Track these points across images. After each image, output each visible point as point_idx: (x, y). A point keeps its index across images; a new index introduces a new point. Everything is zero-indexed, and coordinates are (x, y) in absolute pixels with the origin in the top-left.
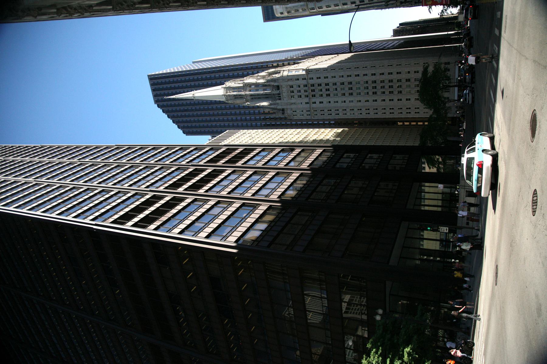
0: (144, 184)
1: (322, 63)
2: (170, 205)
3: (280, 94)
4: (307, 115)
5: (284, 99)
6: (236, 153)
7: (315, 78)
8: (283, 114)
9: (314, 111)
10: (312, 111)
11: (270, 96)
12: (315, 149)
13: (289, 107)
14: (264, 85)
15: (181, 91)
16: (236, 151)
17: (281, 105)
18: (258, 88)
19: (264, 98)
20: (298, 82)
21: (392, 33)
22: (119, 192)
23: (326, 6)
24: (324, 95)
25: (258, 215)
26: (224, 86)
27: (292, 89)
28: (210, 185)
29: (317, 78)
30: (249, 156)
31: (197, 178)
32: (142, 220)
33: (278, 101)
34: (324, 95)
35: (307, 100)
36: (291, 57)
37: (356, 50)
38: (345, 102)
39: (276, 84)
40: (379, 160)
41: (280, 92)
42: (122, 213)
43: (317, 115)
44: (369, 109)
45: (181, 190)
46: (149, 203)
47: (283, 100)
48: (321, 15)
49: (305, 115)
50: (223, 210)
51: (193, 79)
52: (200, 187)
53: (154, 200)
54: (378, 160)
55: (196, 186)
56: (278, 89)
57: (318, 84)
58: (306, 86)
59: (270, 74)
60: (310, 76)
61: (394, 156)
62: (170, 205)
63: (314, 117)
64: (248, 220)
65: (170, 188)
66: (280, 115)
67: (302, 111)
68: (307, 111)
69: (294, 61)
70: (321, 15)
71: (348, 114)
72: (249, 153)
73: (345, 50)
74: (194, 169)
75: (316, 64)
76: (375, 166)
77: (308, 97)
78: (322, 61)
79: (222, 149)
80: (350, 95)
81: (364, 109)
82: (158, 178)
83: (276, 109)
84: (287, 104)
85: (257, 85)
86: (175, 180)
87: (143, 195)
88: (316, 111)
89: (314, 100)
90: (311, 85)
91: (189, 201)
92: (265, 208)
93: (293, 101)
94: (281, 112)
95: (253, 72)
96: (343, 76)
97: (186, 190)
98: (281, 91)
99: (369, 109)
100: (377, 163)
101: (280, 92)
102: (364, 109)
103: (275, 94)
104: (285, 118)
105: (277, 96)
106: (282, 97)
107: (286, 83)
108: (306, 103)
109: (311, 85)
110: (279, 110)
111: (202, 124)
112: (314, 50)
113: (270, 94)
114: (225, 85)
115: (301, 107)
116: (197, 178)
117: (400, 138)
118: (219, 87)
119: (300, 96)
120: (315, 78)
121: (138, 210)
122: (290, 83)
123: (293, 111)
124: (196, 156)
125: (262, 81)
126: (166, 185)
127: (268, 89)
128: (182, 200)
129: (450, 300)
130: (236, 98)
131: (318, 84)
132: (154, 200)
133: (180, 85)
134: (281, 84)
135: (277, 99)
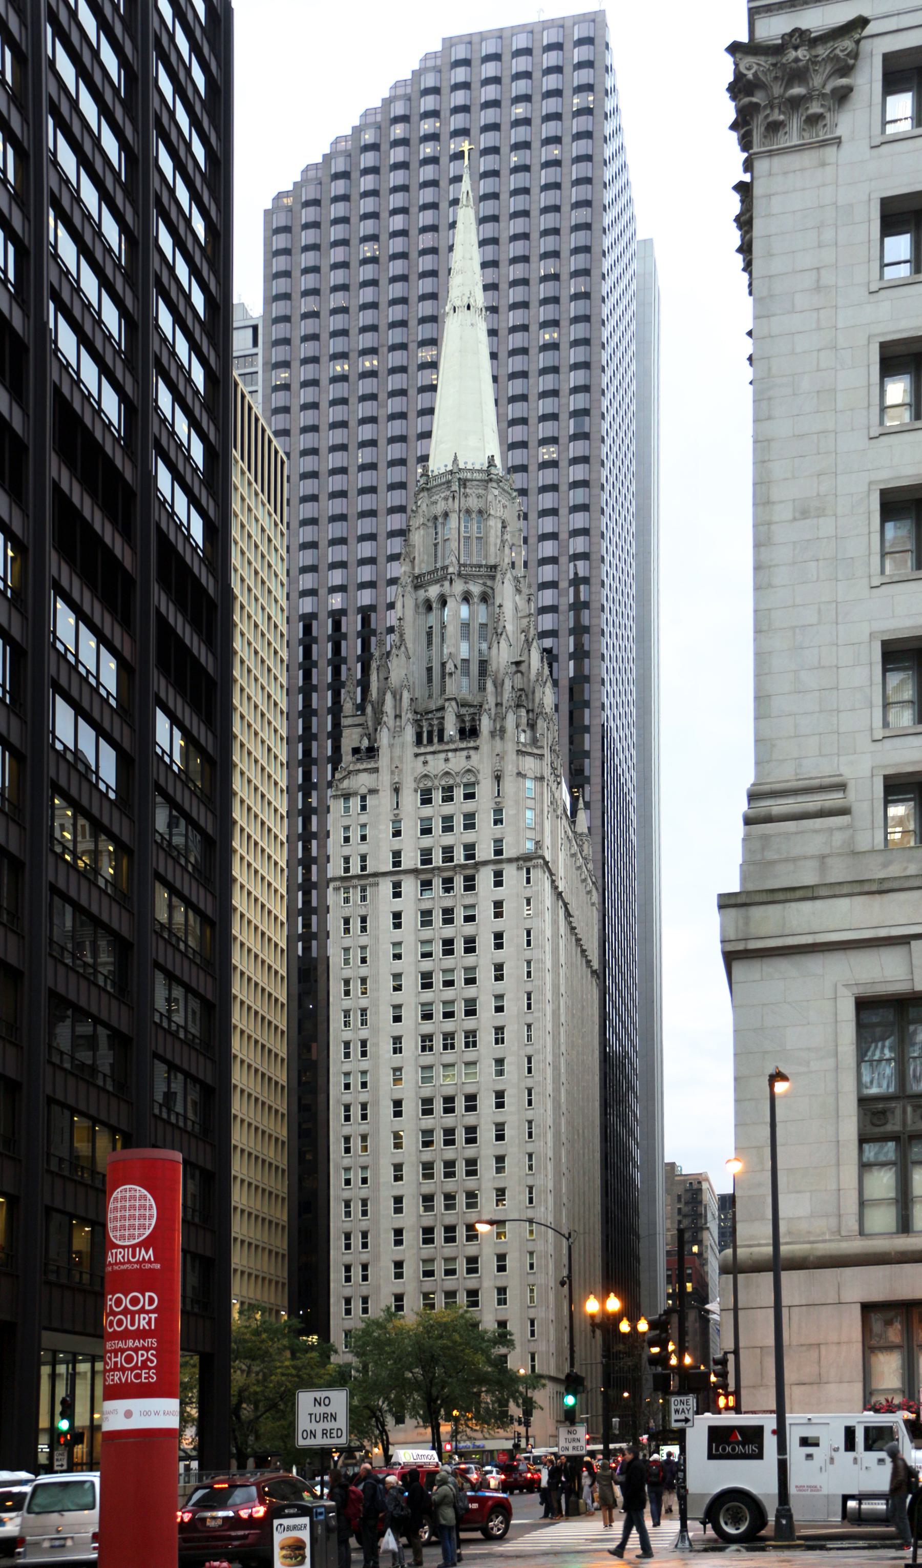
1: (562, 912)
3: (441, 740)
4: (347, 860)
5: (422, 758)
7: (500, 893)
8: (356, 751)
13: (385, 780)
17: (391, 746)
18: (475, 635)
21: (687, 1168)
24: (427, 1027)
34: (427, 1027)
35: (411, 860)
38: (397, 957)
39: (486, 725)
40: (181, 1124)
48: (97, 1530)
53: (120, 518)
54: (181, 1119)
57: (426, 1241)
61: (197, 1173)
66: (351, 738)
76: (177, 1119)
77: (424, 862)
80: (423, 1041)
83: (378, 722)
84: (396, 769)
93: (410, 799)
94: (365, 743)
100: (189, 1123)
101: (452, 741)
104: (336, 760)
105: (431, 725)
106: (430, 749)
110: (372, 738)
115: (383, 836)
117: (277, 1196)
119: (426, 831)
120: (500, 893)
122: (486, 789)
123: (363, 798)
130: (429, 635)
131: (426, 1241)
132: (120, 518)
135: (421, 727)
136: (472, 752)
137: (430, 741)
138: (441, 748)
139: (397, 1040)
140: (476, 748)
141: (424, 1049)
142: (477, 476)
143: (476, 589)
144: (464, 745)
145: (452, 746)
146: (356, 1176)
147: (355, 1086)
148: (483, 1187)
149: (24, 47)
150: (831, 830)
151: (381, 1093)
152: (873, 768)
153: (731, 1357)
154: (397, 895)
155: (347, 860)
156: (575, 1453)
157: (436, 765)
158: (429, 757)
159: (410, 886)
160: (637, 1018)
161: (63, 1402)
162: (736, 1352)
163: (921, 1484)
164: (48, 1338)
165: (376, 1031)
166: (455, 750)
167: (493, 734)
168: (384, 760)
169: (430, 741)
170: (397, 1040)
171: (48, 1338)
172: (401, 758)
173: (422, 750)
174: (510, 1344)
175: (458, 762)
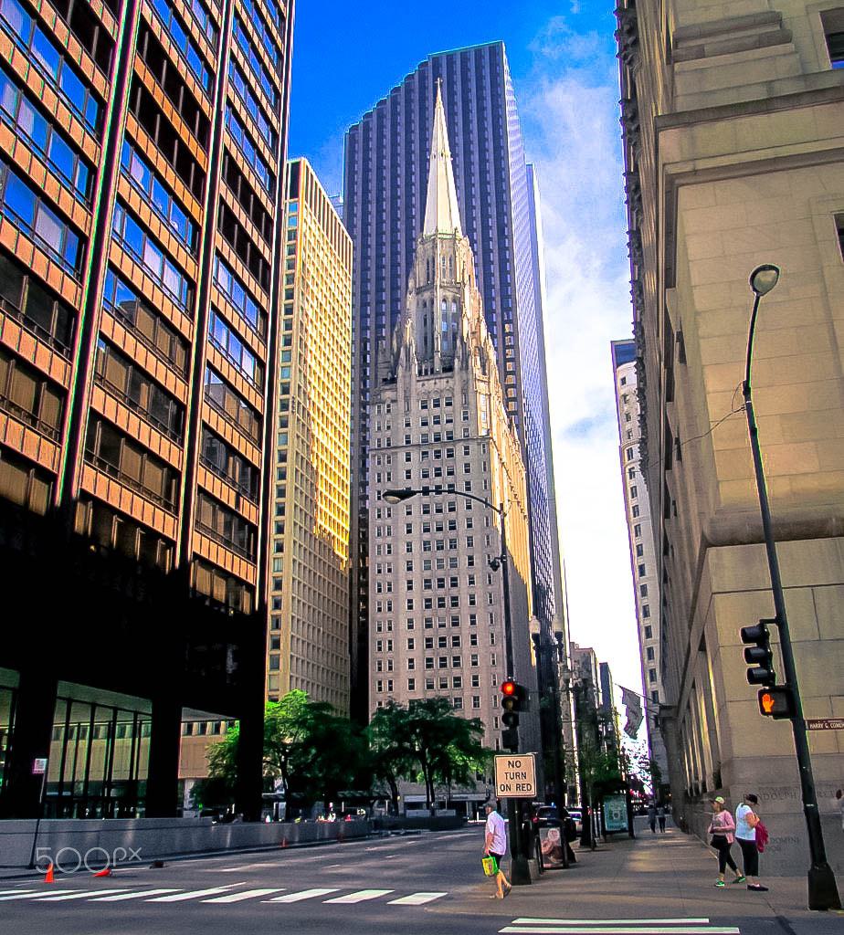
0: (237, 92)
2: (185, 164)
3: (432, 372)
4: (379, 440)
5: (421, 383)
6: (255, 240)
8: (385, 380)
9: (389, 457)
10: (389, 452)
11: (429, 350)
12: (261, 448)
13: (401, 394)
14: (454, 336)
15: (457, 170)
16: (262, 242)
17: (404, 377)
19: (426, 334)
20: (459, 418)
22: (216, 29)
23: (635, 487)
25: (142, 364)
26: (460, 235)
27: (443, 402)
28: (233, 259)
29: (467, 465)
30: (246, 273)
31: (250, 228)
32: (147, 97)
33: (415, 370)
36: (527, 407)
37: (540, 562)
39: (457, 364)
41: (438, 372)
42: (166, 43)
43: (379, 463)
44: (390, 590)
45: (222, 187)
46: (190, 109)
47: (418, 381)
49: (379, 435)
50: (155, 276)
51: (487, 192)
52: (228, 235)
55: (148, 113)
56: (445, 370)
58: (449, 438)
59: (481, 351)
60: (473, 446)
62: (185, 164)
63: (374, 456)
64: (152, 359)
65: (227, 160)
67: (389, 428)
68: (389, 439)
69: (516, 417)
70: (627, 334)
71: (379, 540)
72: (254, 272)
73: (538, 534)
74: (208, 119)
75: (503, 463)
78: (512, 478)
79: (270, 205)
80: (424, 545)
81: (389, 577)
82: (250, 130)
85: (459, 315)
86: (246, 171)
87: (209, 94)
88: (389, 462)
89: (415, 455)
90: (452, 450)
91: (195, 210)
92: (179, 395)
93: (415, 406)
95: (496, 336)
96: (470, 526)
97: (222, 201)
98: (439, 376)
99: (390, 590)
102: (389, 577)
103: (433, 362)
106: (426, 377)
107: (458, 389)
108: (408, 437)
109: (452, 450)
110: (394, 372)
111: (387, 250)
112: (544, 486)
113: (433, 348)
114: (462, 237)
116: (250, 228)
118: (457, 223)
121: (174, 84)
122: (458, 400)
123: (388, 406)
124: (262, 150)
125: (466, 329)
126: (234, 152)
127: (445, 343)
128: (198, 193)
129: (261, 773)
133: (476, 169)
134: (457, 377)
136: (450, 380)
137: (426, 374)
138: (432, 377)
139: (409, 544)
140: (451, 377)
141: (425, 549)
142: (448, 237)
143: (450, 295)
144: (444, 375)
145: (439, 376)
146: (385, 627)
147: (385, 571)
148: (463, 632)
149: (219, 24)
150: (773, 58)
151: (400, 575)
152: (807, 7)
153: (773, 629)
154: (408, 460)
155: (379, 440)
156: (520, 794)
157: (430, 385)
158: (426, 382)
159: (415, 455)
160: (549, 546)
161: (71, 738)
162: (780, 621)
163: (8, 677)
164: (63, 688)
165: (396, 539)
166: (441, 378)
167: (461, 369)
168: (400, 384)
169: (426, 374)
170: (409, 544)
171: (63, 688)
172: (410, 383)
173: (422, 378)
174: (482, 732)
175: (442, 384)
